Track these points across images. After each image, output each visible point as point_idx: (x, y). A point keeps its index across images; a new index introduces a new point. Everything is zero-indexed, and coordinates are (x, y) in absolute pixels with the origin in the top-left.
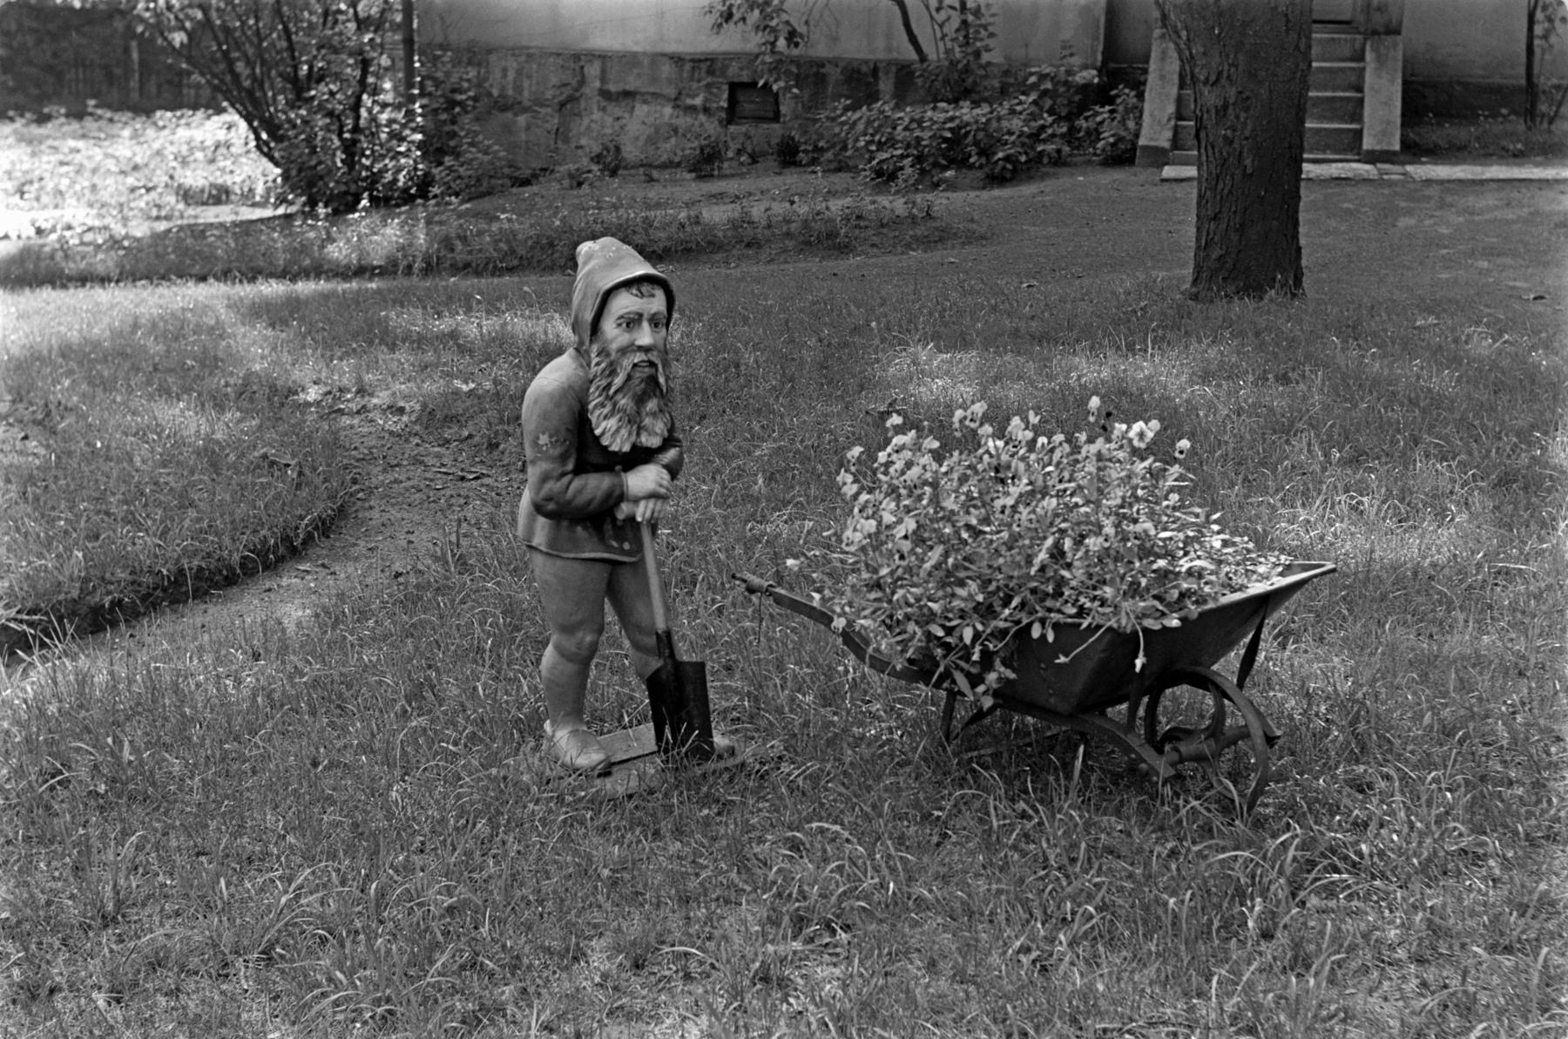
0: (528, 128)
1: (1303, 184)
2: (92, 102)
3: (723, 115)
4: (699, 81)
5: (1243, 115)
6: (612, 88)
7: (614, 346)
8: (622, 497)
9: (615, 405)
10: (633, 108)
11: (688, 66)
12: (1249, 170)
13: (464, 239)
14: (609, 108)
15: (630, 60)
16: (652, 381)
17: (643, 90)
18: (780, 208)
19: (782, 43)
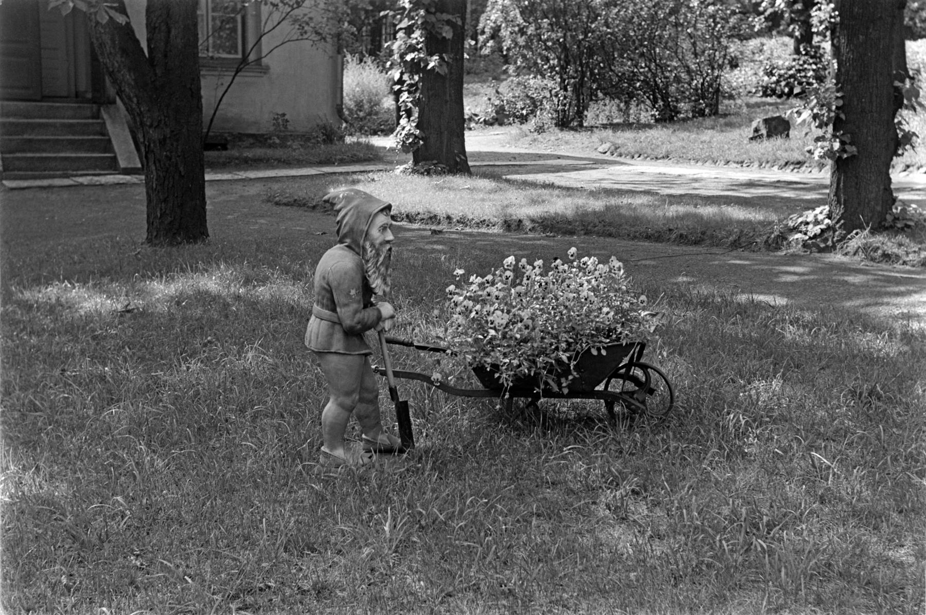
1: (206, 183)
5: (175, 144)
12: (183, 174)
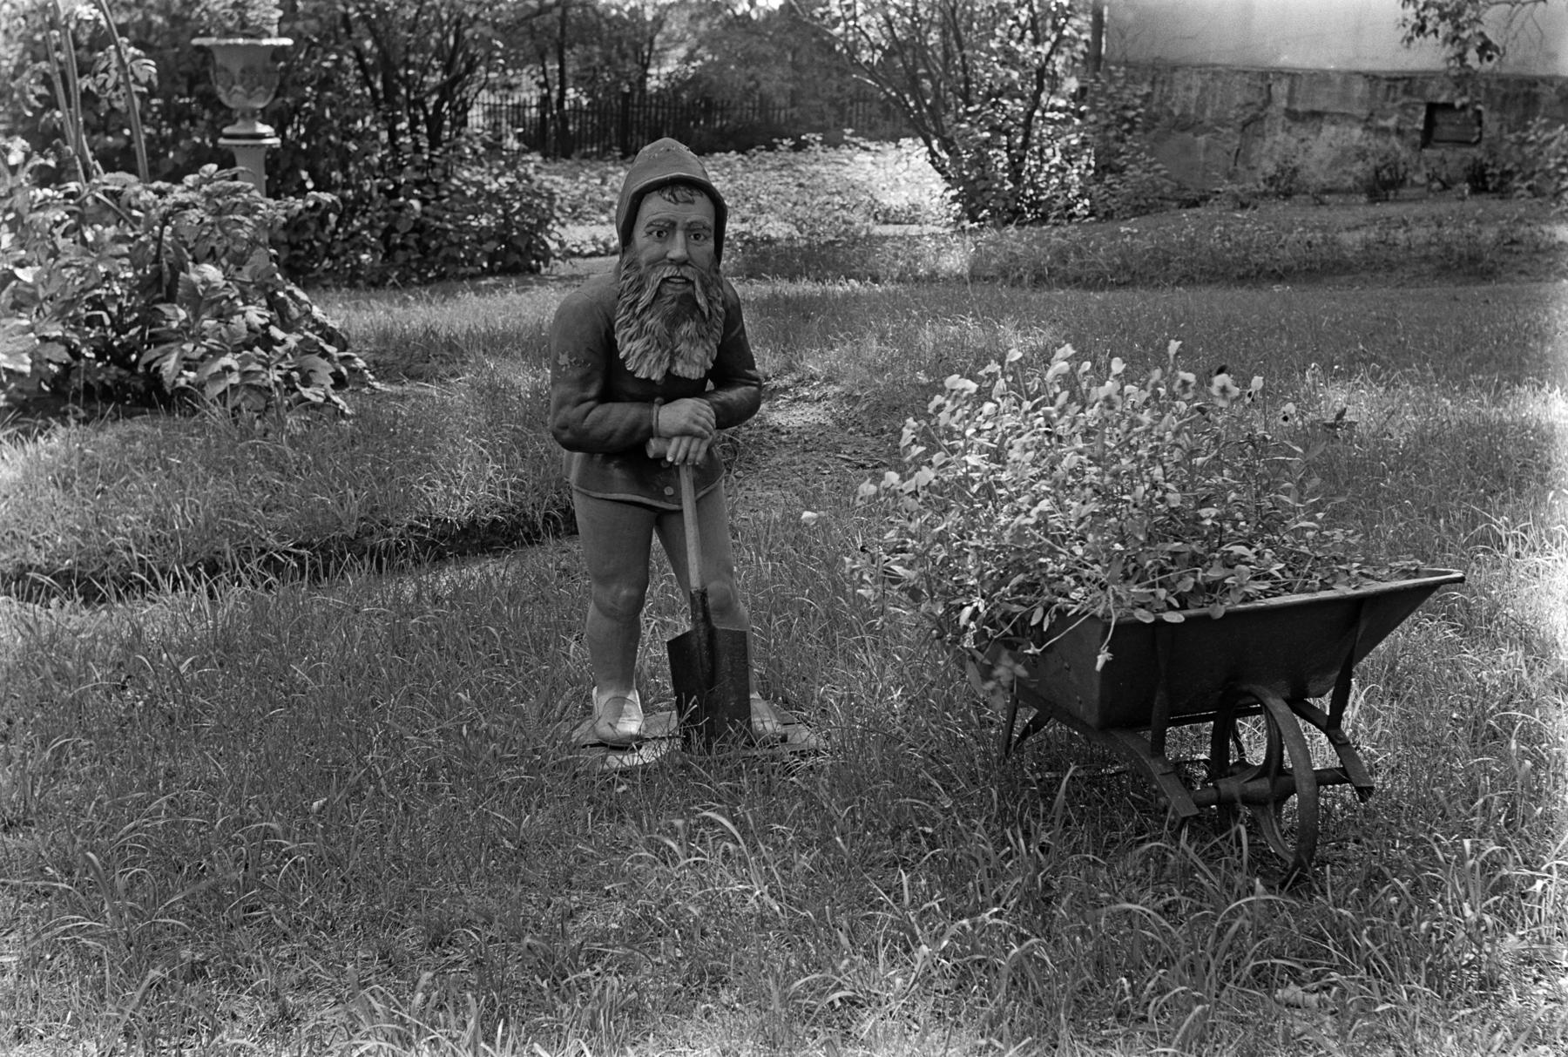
0: (1207, 149)
2: (849, 131)
3: (1418, 138)
4: (1394, 100)
6: (1299, 107)
7: (643, 258)
8: (650, 433)
9: (642, 325)
10: (1320, 130)
11: (1384, 85)
13: (1079, 252)
14: (1294, 130)
15: (1320, 78)
16: (688, 303)
17: (1331, 110)
18: (1421, 233)
19: (1472, 56)
